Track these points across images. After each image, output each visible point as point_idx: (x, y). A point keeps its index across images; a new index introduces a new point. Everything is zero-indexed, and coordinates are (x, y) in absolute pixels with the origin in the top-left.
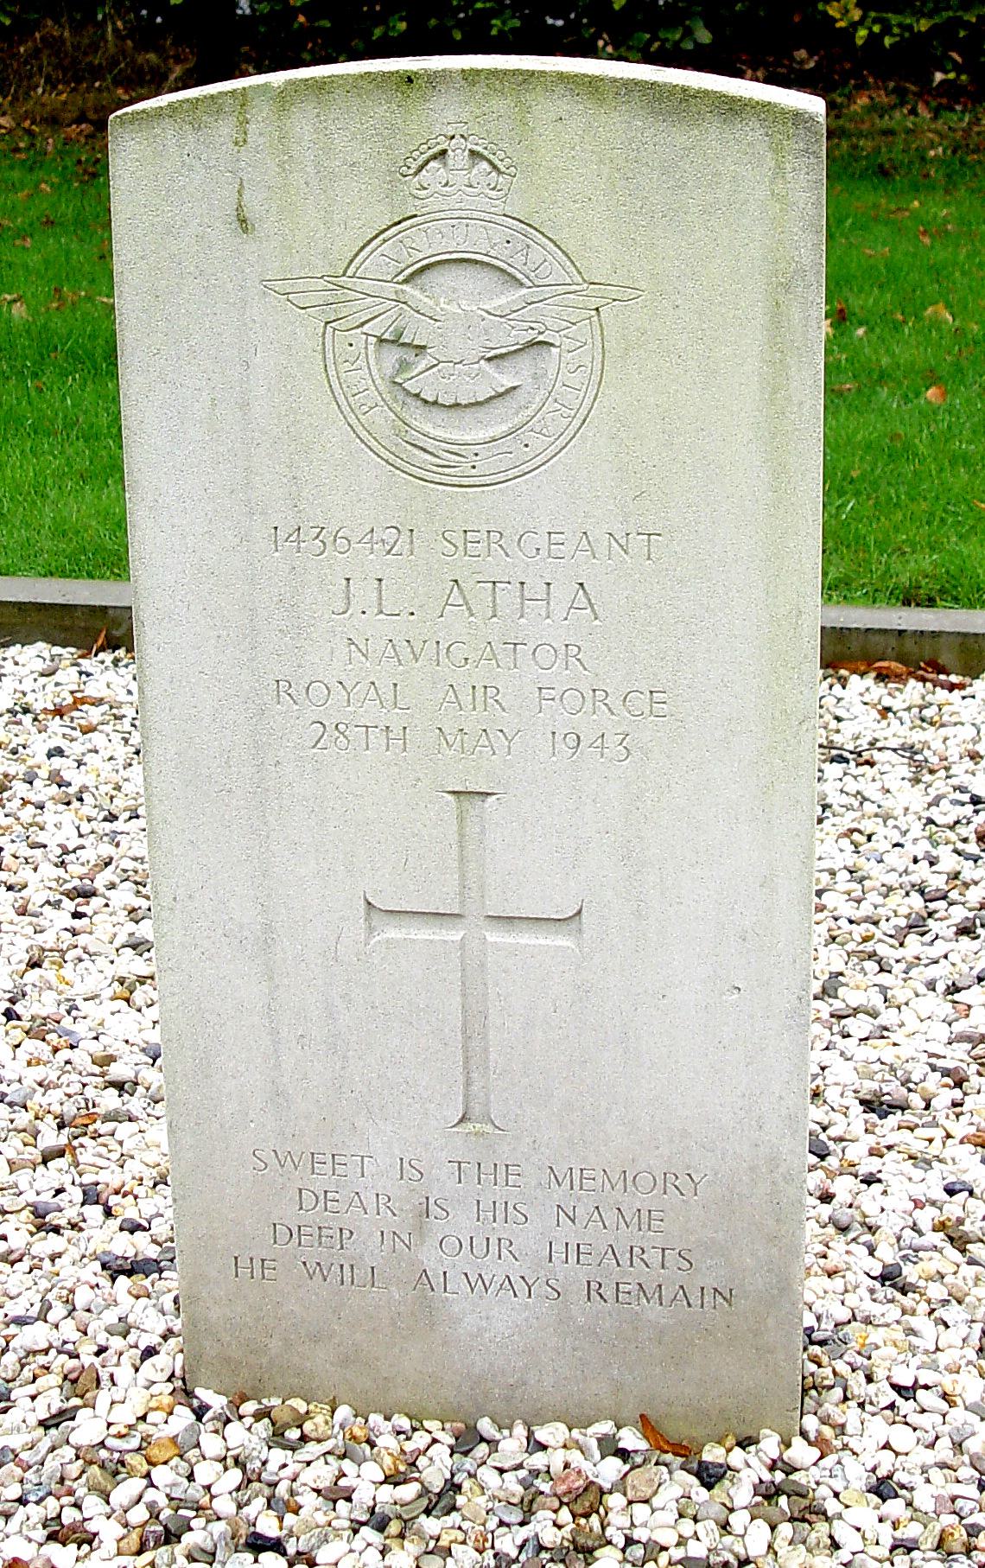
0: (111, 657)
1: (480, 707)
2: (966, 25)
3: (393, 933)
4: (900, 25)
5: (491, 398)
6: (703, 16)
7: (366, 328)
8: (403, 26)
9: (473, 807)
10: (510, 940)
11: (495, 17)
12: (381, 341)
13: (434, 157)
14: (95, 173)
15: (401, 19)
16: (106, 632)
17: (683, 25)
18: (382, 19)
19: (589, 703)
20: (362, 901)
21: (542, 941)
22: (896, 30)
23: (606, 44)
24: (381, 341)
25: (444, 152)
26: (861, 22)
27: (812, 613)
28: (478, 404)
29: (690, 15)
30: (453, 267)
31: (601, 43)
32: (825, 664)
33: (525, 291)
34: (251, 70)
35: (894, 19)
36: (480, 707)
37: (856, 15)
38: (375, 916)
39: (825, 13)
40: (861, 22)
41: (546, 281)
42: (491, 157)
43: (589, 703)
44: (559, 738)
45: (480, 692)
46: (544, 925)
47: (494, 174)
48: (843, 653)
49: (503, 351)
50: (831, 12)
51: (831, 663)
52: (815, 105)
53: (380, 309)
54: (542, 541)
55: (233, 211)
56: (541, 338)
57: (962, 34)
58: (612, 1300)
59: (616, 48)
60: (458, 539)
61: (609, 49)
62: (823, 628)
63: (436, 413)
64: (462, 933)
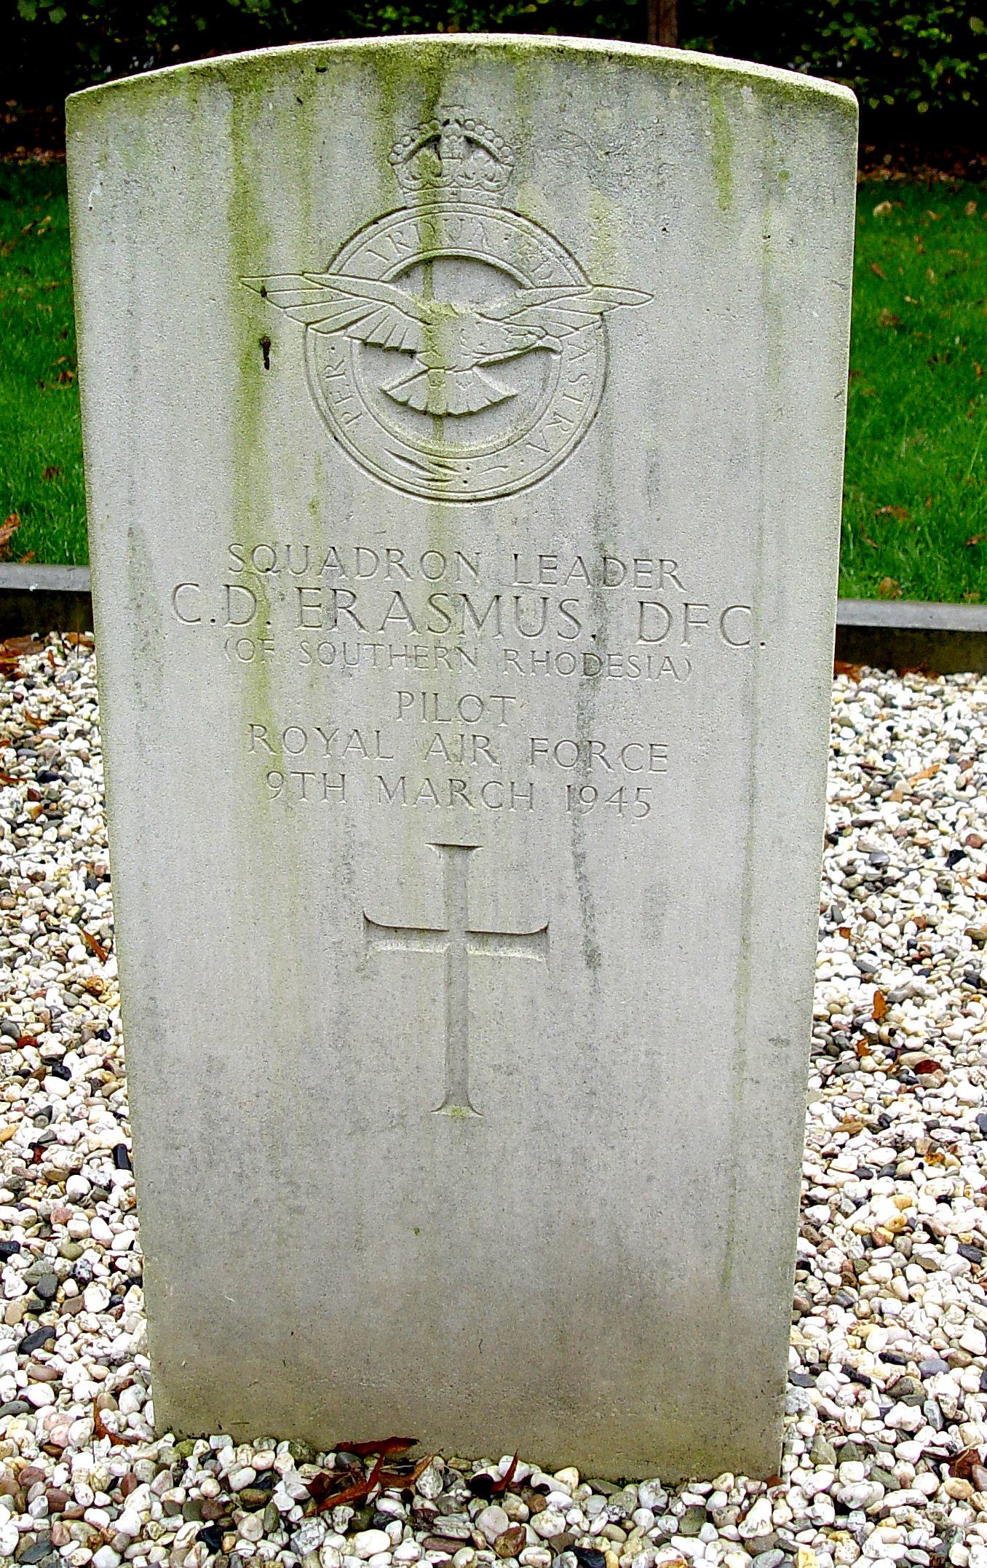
3: (388, 946)
9: (458, 858)
12: (365, 343)
20: (362, 919)
24: (365, 343)
28: (471, 414)
30: (454, 265)
42: (488, 144)
47: (492, 162)
48: (859, 649)
49: (501, 356)
52: (844, 93)
55: (160, 179)
56: (540, 343)
62: (838, 626)
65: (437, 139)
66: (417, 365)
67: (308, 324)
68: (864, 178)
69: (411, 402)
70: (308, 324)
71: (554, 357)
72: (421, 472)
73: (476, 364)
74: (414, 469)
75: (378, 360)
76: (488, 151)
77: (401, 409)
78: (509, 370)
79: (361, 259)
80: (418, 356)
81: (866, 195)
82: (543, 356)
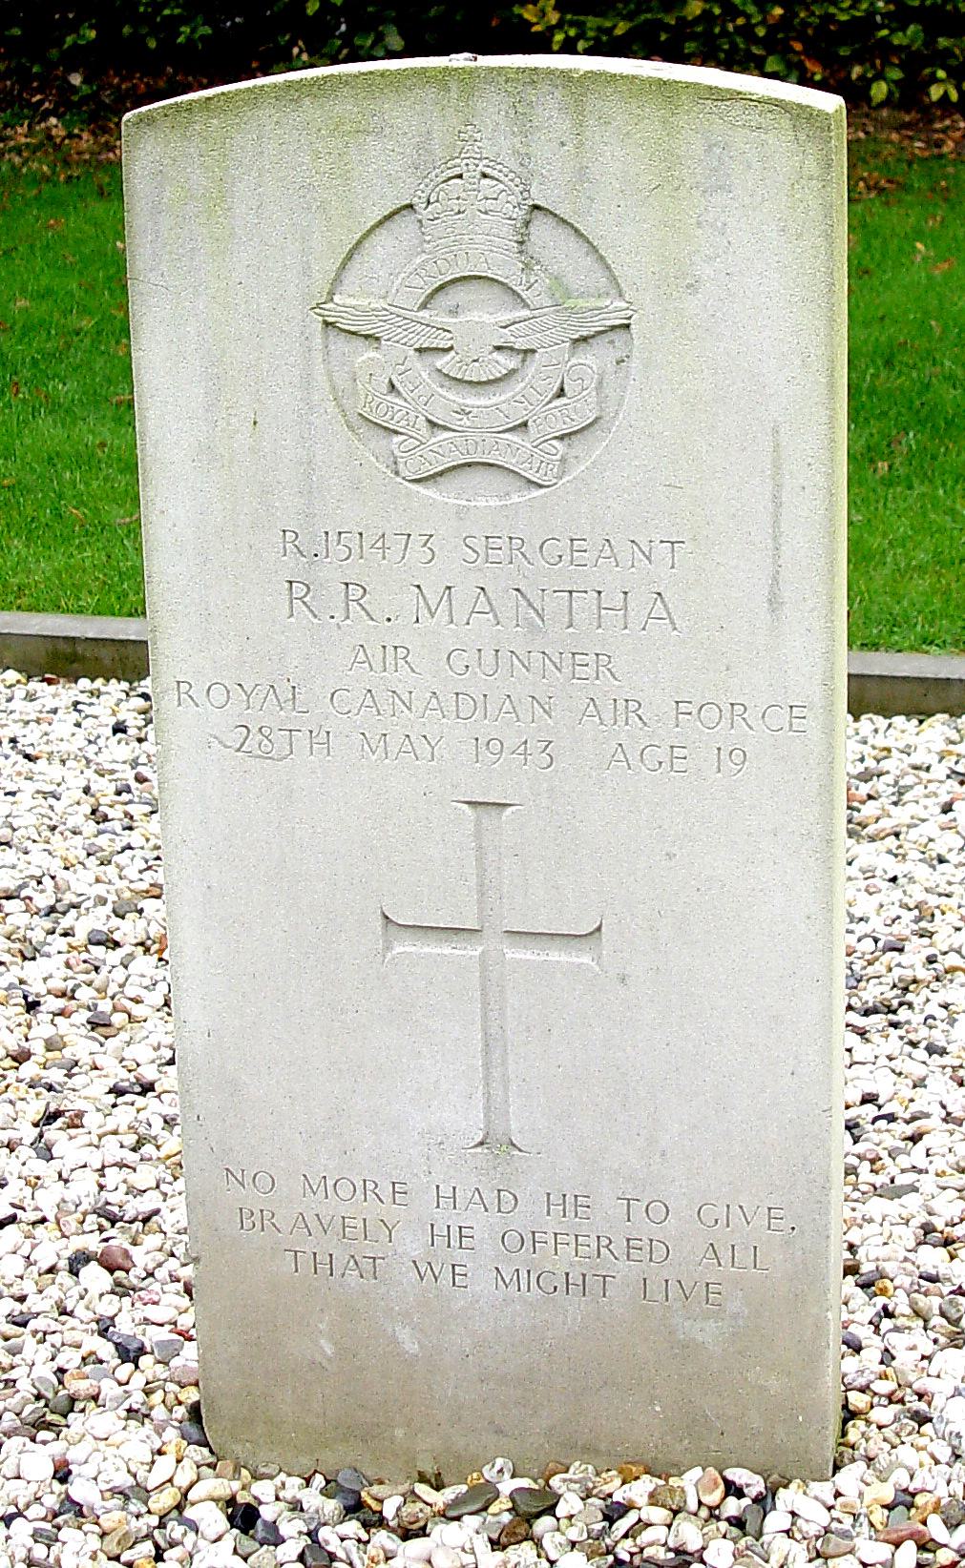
0: (866, 763)
2: (667, 28)
4: (600, 29)
6: (395, 22)
8: (93, 34)
11: (185, 24)
14: (106, 181)
15: (91, 27)
16: (128, 662)
17: (375, 29)
18: (74, 27)
21: (529, 956)
22: (591, 34)
23: (301, 51)
26: (560, 25)
27: (844, 662)
29: (384, 21)
31: (296, 51)
34: (395, 42)
35: (592, 22)
37: (554, 18)
38: (392, 928)
39: (520, 16)
40: (560, 25)
48: (869, 697)
50: (526, 16)
51: (856, 710)
52: (831, 103)
55: (255, 221)
57: (663, 37)
58: (387, 1200)
59: (310, 55)
61: (305, 57)
64: (480, 949)
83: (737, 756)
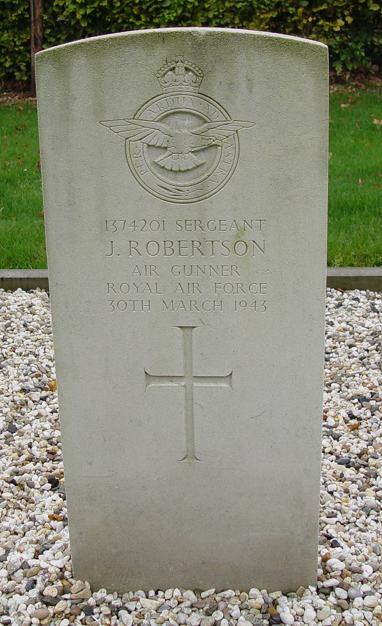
1: (191, 292)
5: (194, 168)
7: (142, 140)
9: (188, 331)
10: (205, 385)
12: (148, 145)
13: (171, 70)
16: (43, 284)
19: (235, 289)
24: (148, 145)
25: (174, 68)
27: (325, 272)
28: (189, 170)
32: (47, 278)
33: (207, 124)
36: (191, 292)
41: (217, 120)
43: (235, 289)
44: (238, 303)
45: (148, 267)
46: (202, 379)
47: (195, 77)
53: (149, 132)
54: (217, 223)
55: (98, 104)
56: (214, 143)
60: (183, 225)
63: (180, 176)
65: (174, 68)
66: (168, 153)
67: (127, 139)
68: (214, 22)
69: (173, 169)
70: (127, 139)
71: (220, 148)
72: (169, 192)
73: (191, 151)
74: (166, 191)
75: (153, 151)
76: (193, 72)
77: (161, 170)
78: (202, 154)
79: (146, 114)
80: (168, 149)
81: (335, 80)
82: (213, 149)
83: (243, 304)
